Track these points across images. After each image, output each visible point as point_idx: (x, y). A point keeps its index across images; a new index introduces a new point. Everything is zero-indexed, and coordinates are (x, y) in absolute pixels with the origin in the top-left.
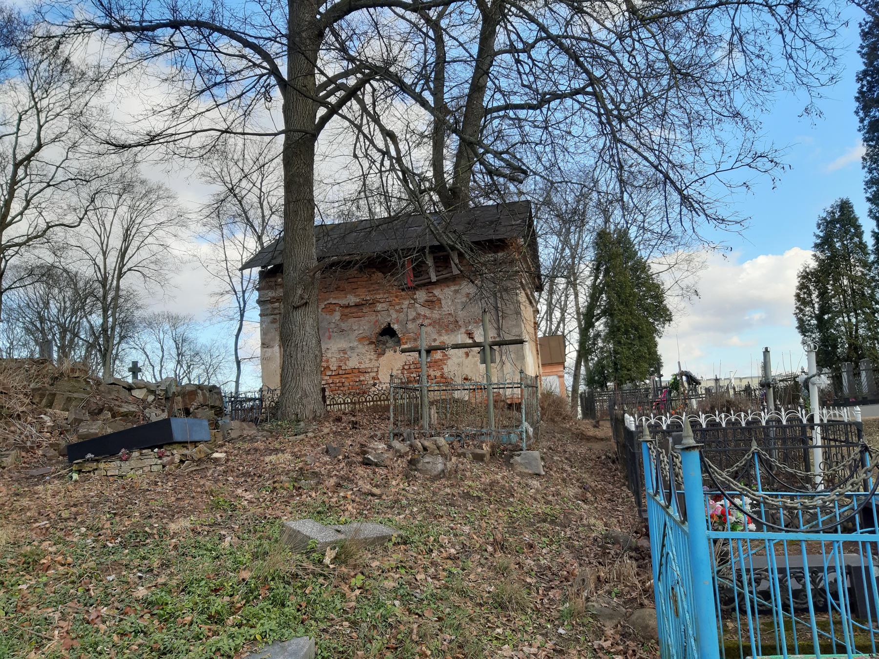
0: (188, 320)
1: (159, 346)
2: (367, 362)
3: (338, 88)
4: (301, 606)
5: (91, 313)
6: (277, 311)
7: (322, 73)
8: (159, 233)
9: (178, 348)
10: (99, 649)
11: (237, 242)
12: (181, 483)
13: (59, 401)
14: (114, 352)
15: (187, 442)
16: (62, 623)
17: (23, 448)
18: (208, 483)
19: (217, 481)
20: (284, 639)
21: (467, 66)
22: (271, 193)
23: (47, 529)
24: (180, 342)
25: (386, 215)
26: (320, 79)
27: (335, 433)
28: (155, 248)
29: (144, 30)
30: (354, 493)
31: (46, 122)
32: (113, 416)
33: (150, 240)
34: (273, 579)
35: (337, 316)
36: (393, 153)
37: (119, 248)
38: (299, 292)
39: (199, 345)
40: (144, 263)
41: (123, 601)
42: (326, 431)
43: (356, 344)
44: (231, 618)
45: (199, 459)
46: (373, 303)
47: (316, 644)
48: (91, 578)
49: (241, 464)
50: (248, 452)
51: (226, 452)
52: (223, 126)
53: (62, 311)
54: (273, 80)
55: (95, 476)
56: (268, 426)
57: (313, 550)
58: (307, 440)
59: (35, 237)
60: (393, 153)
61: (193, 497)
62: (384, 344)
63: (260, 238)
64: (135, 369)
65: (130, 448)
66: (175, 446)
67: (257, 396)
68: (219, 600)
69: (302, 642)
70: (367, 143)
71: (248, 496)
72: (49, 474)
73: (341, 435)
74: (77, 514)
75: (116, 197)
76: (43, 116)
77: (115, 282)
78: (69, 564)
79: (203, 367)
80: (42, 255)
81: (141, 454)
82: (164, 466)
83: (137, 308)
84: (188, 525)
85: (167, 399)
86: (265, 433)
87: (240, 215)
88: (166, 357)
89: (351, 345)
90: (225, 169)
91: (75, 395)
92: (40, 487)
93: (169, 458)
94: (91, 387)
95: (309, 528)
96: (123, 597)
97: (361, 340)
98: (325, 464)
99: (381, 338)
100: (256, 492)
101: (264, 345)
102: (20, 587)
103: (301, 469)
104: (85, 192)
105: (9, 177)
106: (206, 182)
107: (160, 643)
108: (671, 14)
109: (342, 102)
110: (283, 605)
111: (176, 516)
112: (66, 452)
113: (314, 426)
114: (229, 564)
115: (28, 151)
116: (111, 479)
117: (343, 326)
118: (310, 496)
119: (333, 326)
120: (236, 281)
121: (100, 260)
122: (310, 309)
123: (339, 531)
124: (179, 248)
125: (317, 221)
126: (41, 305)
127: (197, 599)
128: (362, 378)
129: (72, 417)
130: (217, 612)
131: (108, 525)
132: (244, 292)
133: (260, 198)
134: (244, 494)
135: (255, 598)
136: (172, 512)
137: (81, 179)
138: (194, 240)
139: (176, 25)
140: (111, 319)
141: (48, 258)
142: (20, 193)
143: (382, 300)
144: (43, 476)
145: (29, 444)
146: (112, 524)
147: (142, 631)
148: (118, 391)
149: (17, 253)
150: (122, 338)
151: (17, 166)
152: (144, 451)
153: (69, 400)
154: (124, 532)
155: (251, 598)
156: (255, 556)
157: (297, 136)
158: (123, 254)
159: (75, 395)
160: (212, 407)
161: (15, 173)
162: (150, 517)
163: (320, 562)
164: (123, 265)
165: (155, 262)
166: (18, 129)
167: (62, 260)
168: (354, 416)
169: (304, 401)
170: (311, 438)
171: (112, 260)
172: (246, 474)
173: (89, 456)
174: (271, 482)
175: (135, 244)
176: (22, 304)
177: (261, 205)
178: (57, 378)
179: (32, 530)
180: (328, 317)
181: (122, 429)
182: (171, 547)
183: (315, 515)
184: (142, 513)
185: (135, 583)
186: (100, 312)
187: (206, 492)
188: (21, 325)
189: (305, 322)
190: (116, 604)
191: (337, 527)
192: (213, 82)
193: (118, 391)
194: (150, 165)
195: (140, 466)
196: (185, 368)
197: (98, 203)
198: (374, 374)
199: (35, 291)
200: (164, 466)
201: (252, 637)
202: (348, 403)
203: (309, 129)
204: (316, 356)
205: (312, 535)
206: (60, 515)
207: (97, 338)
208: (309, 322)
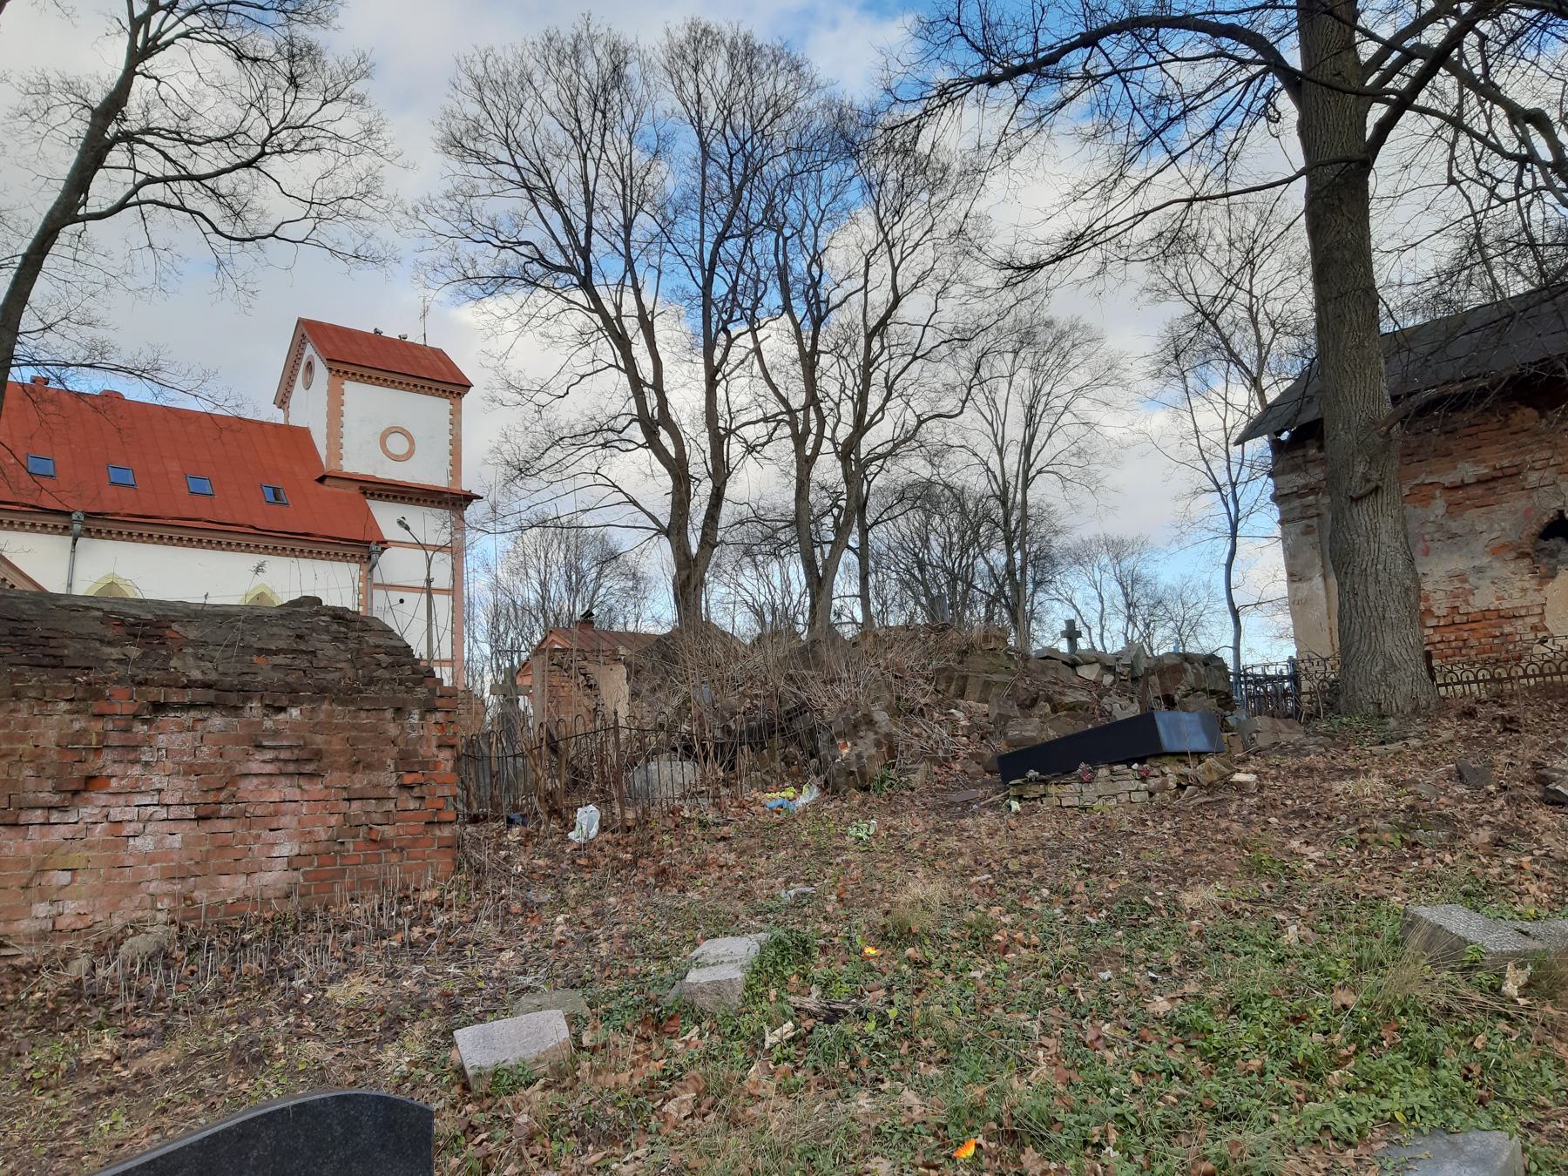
0: (1139, 545)
1: (1094, 593)
2: (1517, 595)
3: (1408, 56)
4: (1470, 1071)
5: (989, 547)
6: (1313, 511)
7: (1373, 37)
8: (1081, 404)
9: (1126, 595)
10: (1112, 1091)
11: (1214, 397)
12: (1186, 824)
13: (973, 688)
14: (1028, 608)
15: (1186, 754)
16: (1045, 1041)
17: (934, 760)
18: (1235, 825)
19: (1248, 824)
20: (1452, 1129)
22: (1272, 295)
23: (991, 887)
24: (1130, 584)
26: (1367, 50)
27: (1465, 740)
28: (1074, 431)
29: (1042, 65)
30: (1536, 861)
31: (902, 260)
32: (1054, 710)
33: (1067, 418)
34: (1404, 1013)
35: (1439, 507)
36: (1545, 154)
37: (1020, 439)
38: (1361, 469)
39: (1161, 588)
40: (1061, 457)
41: (1132, 1016)
42: (1446, 735)
43: (1486, 560)
44: (1336, 1073)
45: (1210, 784)
47: (1525, 1150)
48: (1074, 972)
49: (1288, 796)
50: (1296, 774)
51: (1255, 772)
52: (1187, 193)
53: (947, 548)
54: (1272, 81)
55: (1044, 806)
56: (1323, 725)
57: (1474, 966)
58: (1408, 752)
59: (904, 442)
60: (1545, 154)
61: (1213, 850)
62: (1552, 554)
63: (1256, 382)
64: (1071, 634)
65: (1094, 762)
66: (1165, 760)
67: (1285, 673)
68: (1305, 1038)
69: (1494, 1142)
70: (1478, 146)
71: (1314, 853)
72: (977, 801)
73: (1479, 744)
74: (1030, 866)
75: (1009, 357)
76: (897, 251)
77: (1019, 496)
78: (1035, 946)
79: (1171, 624)
80: (914, 467)
81: (1112, 772)
82: (1151, 794)
83: (1056, 533)
84: (1213, 896)
85: (1135, 679)
86: (1320, 739)
87: (1216, 348)
88: (1107, 610)
89: (1477, 563)
90: (1183, 271)
91: (995, 678)
92: (969, 821)
93: (1158, 781)
94: (1016, 664)
95: (1458, 920)
96: (1132, 1009)
97: (1497, 551)
98: (1460, 799)
99: (1543, 544)
100: (1326, 847)
101: (1293, 577)
102: (973, 974)
103: (1411, 808)
104: (965, 357)
105: (861, 357)
106: (1153, 301)
107: (1215, 1098)
109: (1419, 83)
110: (1433, 1063)
111: (1190, 881)
112: (995, 766)
113: (1418, 726)
114: (1310, 973)
115: (882, 312)
116: (1069, 812)
117: (1454, 526)
118: (1442, 861)
119: (1430, 528)
120: (1218, 467)
121: (994, 463)
122: (1384, 499)
123: (1526, 934)
124: (1113, 425)
125: (1387, 327)
126: (919, 544)
127: (1266, 1031)
128: (1507, 629)
129: (994, 713)
130: (1307, 1059)
131: (1080, 888)
132: (1234, 485)
133: (1250, 310)
134: (1304, 849)
135: (1374, 1043)
136: (1183, 875)
137: (962, 339)
138: (1138, 405)
139: (1089, 40)
140: (1018, 555)
141: (924, 471)
142: (878, 377)
143: (1537, 465)
144: (968, 803)
145: (941, 754)
146: (1087, 886)
147: (1177, 1074)
148: (1056, 670)
149: (882, 468)
150: (1038, 584)
151: (869, 338)
152: (1116, 768)
153: (987, 685)
154: (1112, 901)
155: (1366, 1042)
156: (1359, 967)
157: (1330, 173)
158: (1027, 449)
159: (995, 678)
160: (1213, 692)
161: (868, 348)
162: (1147, 878)
163: (1496, 990)
164: (1030, 466)
165: (1079, 454)
166: (866, 281)
167: (942, 470)
168: (1502, 706)
169: (1391, 679)
170: (1416, 749)
171: (1012, 459)
172: (1301, 813)
173: (1032, 773)
174: (1354, 829)
175: (1043, 429)
176: (893, 544)
177: (1255, 322)
178: (965, 652)
179: (971, 887)
180: (1419, 511)
181: (1070, 731)
182: (1192, 934)
183: (1461, 897)
184: (1131, 872)
185: (1147, 988)
186: (1002, 545)
187: (1235, 842)
188: (894, 575)
189: (1378, 528)
190: (1123, 1020)
191: (1518, 926)
192: (1160, 123)
193: (1056, 670)
194: (1065, 296)
195: (1114, 792)
196: (1142, 628)
197: (984, 373)
198: (1536, 620)
199: (906, 524)
200: (1151, 794)
201: (1388, 1115)
202: (1485, 681)
203: (1355, 154)
204: (1407, 589)
205: (1472, 937)
206: (1006, 866)
207: (1001, 587)
208: (1386, 525)
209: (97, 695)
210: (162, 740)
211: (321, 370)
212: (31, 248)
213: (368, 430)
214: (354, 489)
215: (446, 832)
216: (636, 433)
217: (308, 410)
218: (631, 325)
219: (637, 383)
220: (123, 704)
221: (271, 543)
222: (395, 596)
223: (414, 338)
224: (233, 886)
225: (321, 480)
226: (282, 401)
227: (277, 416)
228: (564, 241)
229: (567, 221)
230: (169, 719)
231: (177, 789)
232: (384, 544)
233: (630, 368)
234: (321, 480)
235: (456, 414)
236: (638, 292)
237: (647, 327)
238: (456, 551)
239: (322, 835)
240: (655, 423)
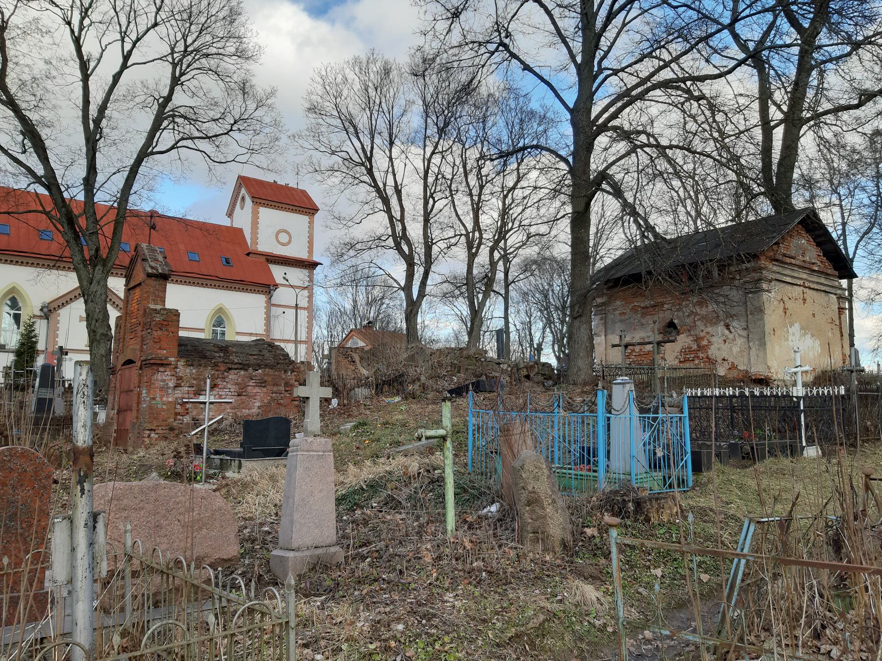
17: (438, 392)
46: (663, 304)
108: (351, 390)
153: (467, 369)
209: (217, 366)
210: (230, 377)
211: (248, 200)
212: (135, 162)
213: (271, 231)
214: (263, 259)
215: (296, 403)
216: (391, 242)
217: (242, 219)
218: (390, 191)
219: (391, 218)
220: (222, 367)
221: (225, 284)
222: (282, 310)
223: (293, 185)
224: (246, 412)
225: (248, 254)
226: (230, 214)
227: (225, 222)
228: (360, 151)
229: (362, 145)
230: (232, 371)
231: (234, 388)
232: (276, 286)
233: (388, 211)
234: (248, 254)
235: (311, 223)
236: (394, 175)
237: (398, 192)
238: (309, 288)
239: (266, 401)
240: (400, 239)
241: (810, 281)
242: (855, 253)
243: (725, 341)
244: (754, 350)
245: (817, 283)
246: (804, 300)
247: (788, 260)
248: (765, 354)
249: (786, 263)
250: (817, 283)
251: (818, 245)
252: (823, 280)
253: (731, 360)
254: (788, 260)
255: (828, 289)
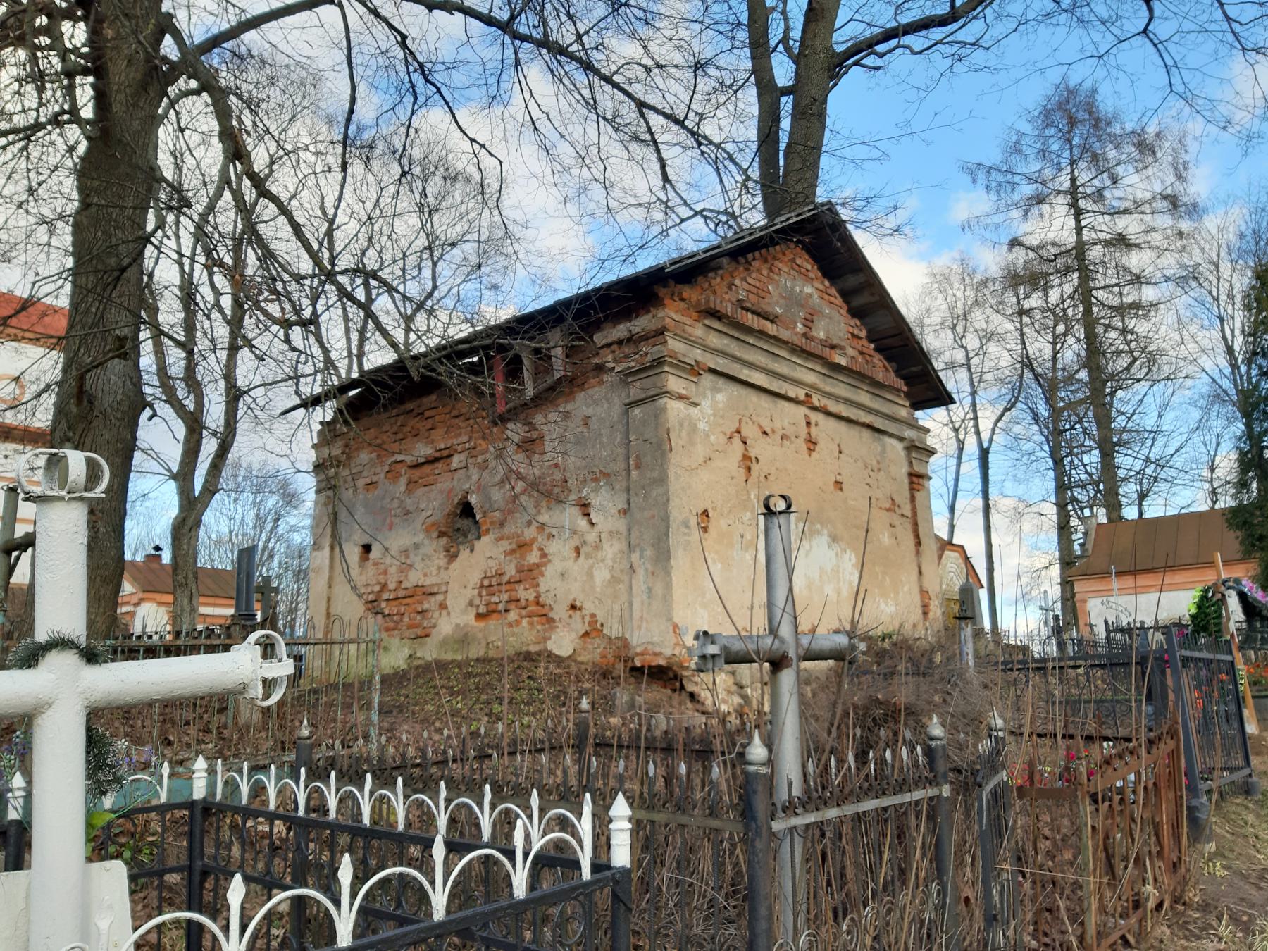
21: (419, 113)
25: (1096, 452)
241: (828, 395)
242: (991, 440)
243: (578, 551)
244: (641, 573)
245: (849, 402)
246: (812, 443)
247: (752, 321)
248: (668, 586)
249: (749, 330)
250: (849, 402)
251: (855, 313)
252: (864, 398)
253: (589, 607)
254: (752, 321)
255: (879, 423)
